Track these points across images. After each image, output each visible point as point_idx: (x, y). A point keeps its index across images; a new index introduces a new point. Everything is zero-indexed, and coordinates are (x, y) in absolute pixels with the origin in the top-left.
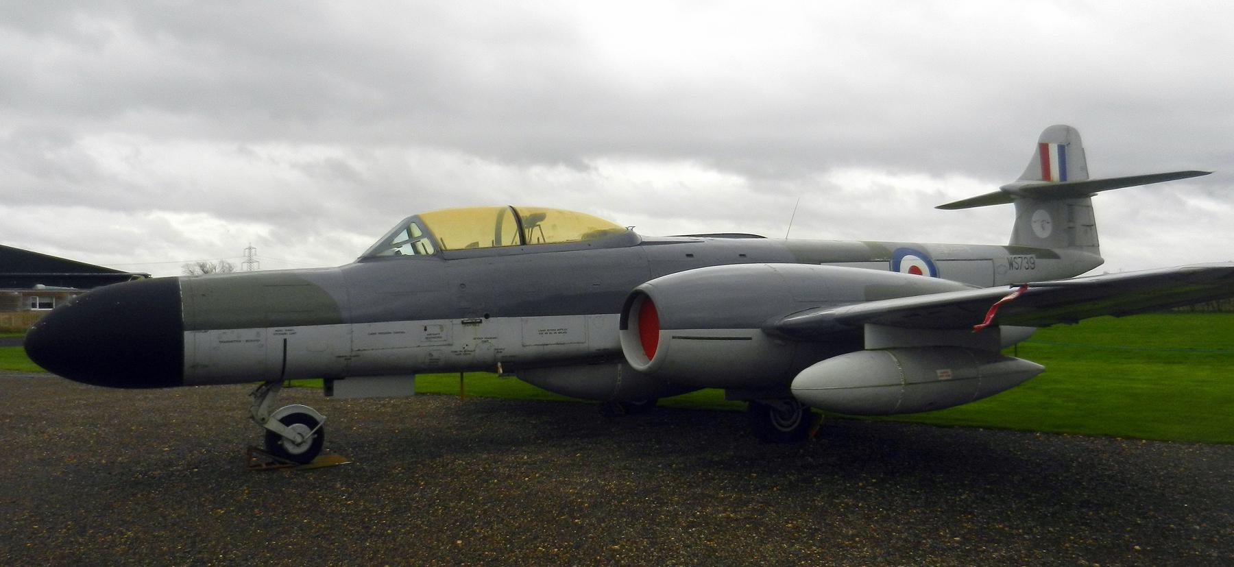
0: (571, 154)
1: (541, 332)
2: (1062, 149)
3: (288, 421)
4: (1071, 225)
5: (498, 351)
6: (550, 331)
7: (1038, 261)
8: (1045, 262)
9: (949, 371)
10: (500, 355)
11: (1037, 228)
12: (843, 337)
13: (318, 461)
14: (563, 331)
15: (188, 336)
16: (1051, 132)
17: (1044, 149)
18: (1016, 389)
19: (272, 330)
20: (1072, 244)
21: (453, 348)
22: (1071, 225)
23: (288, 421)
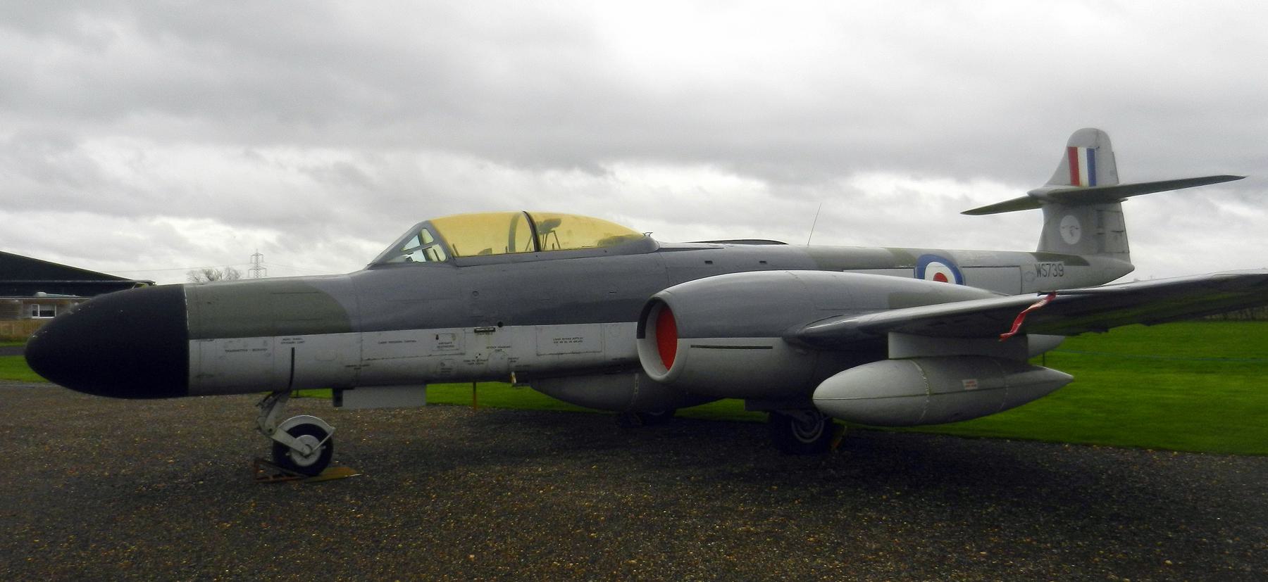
0: (587, 158)
1: (556, 341)
2: (1091, 153)
3: (296, 432)
4: (1101, 231)
5: (512, 360)
6: (565, 340)
7: (1066, 268)
8: (1074, 269)
9: (976, 381)
10: (513, 365)
11: (1065, 234)
12: (866, 346)
13: (327, 473)
14: (579, 340)
15: (193, 345)
16: (1080, 136)
17: (1072, 153)
18: (1044, 400)
19: (279, 339)
20: (1101, 250)
21: (466, 357)
22: (1101, 231)
23: (296, 432)
